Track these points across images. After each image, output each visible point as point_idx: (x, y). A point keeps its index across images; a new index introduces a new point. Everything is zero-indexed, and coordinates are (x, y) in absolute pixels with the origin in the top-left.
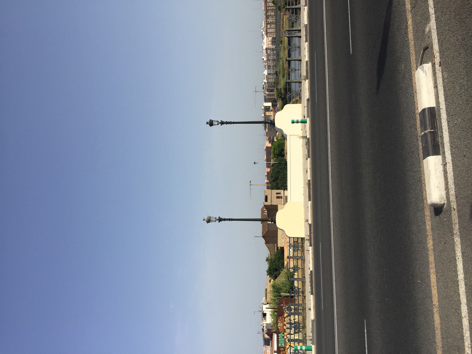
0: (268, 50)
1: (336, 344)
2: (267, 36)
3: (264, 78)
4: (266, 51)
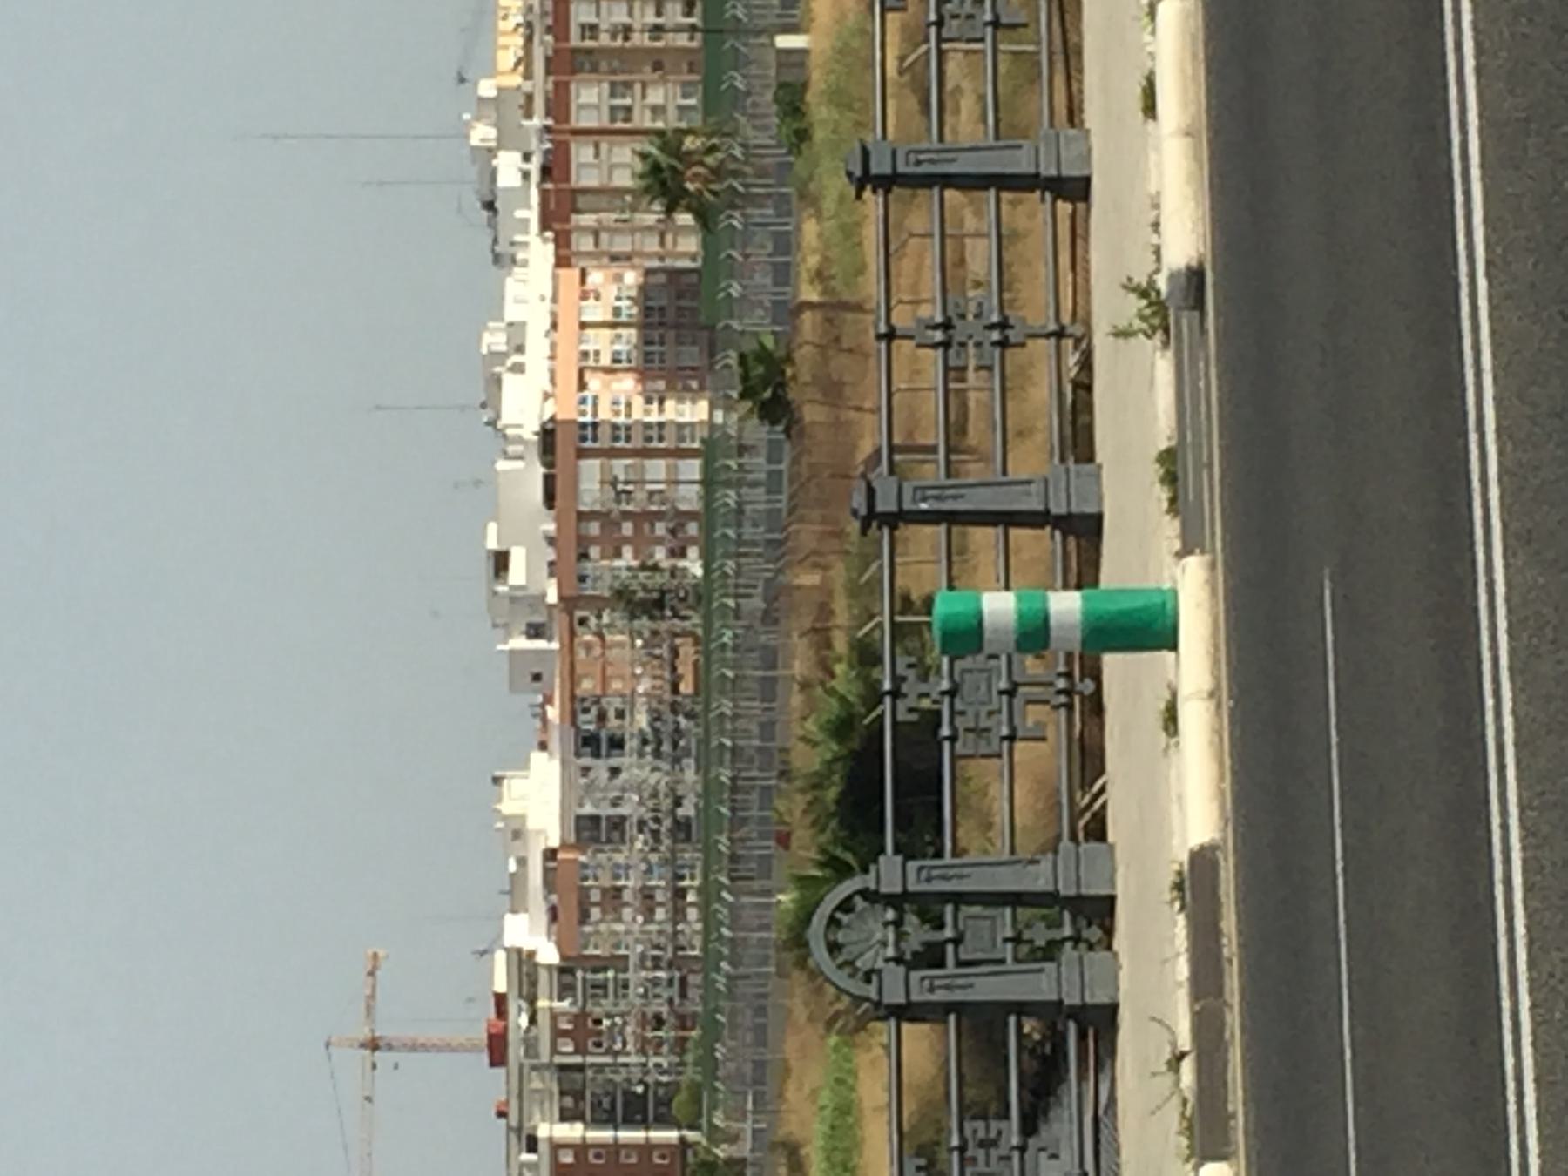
0: (582, 454)
1: (1489, 702)
2: (562, 242)
3: (516, 884)
4: (549, 481)
